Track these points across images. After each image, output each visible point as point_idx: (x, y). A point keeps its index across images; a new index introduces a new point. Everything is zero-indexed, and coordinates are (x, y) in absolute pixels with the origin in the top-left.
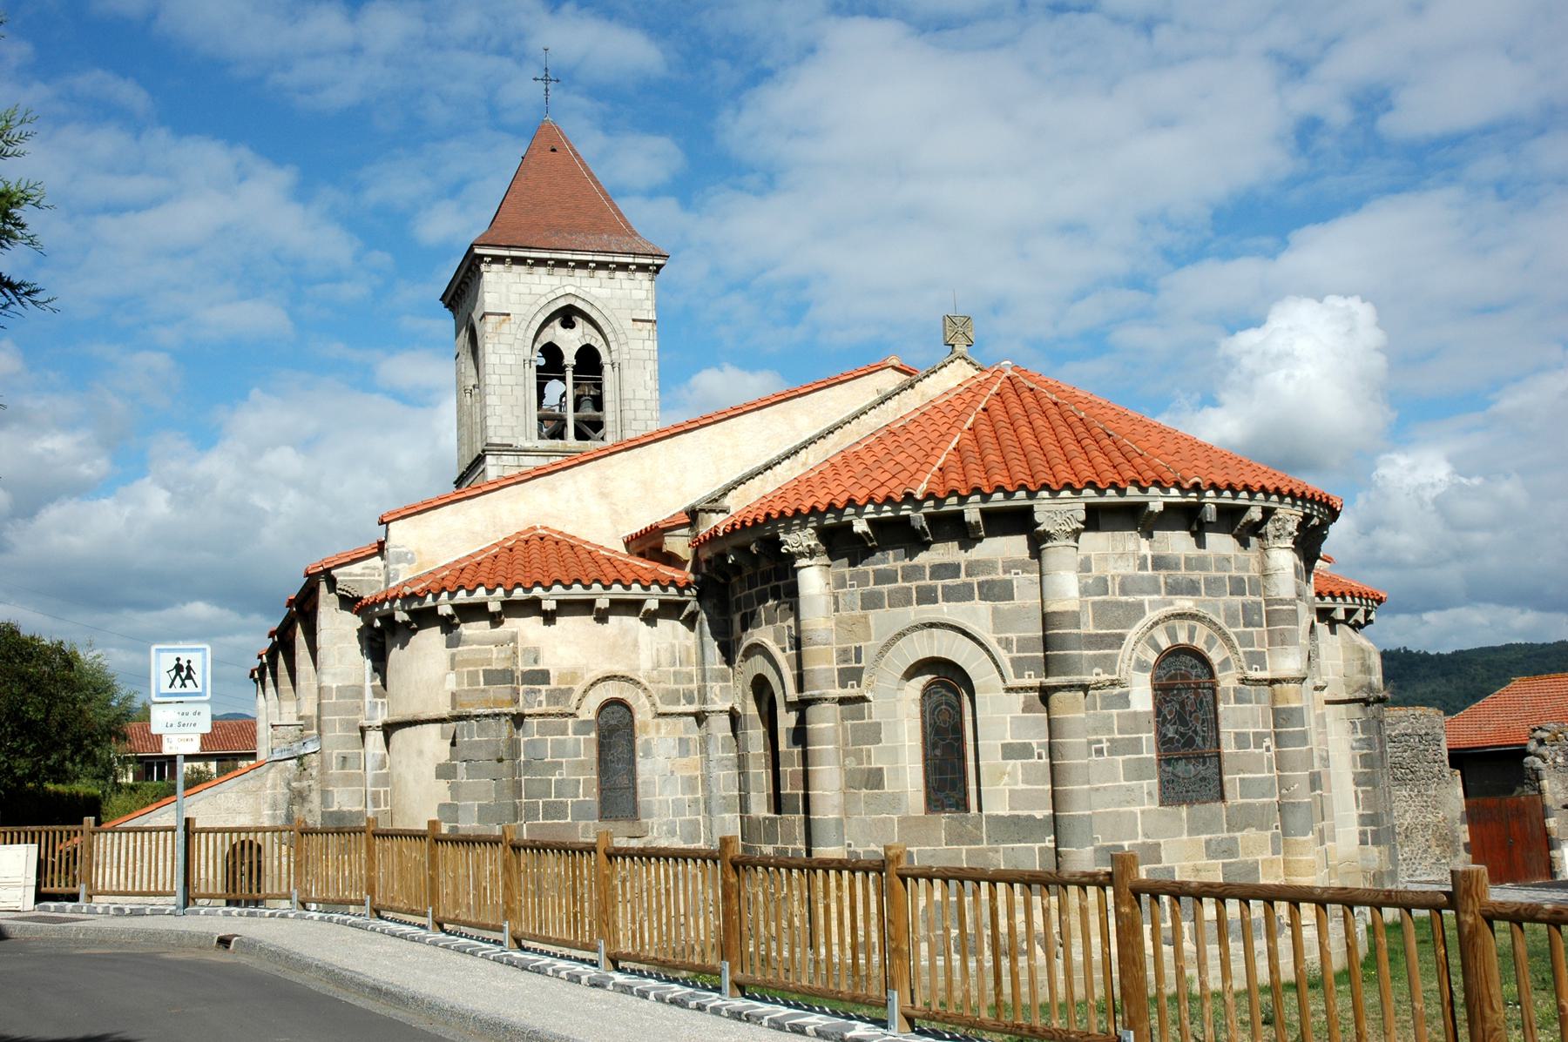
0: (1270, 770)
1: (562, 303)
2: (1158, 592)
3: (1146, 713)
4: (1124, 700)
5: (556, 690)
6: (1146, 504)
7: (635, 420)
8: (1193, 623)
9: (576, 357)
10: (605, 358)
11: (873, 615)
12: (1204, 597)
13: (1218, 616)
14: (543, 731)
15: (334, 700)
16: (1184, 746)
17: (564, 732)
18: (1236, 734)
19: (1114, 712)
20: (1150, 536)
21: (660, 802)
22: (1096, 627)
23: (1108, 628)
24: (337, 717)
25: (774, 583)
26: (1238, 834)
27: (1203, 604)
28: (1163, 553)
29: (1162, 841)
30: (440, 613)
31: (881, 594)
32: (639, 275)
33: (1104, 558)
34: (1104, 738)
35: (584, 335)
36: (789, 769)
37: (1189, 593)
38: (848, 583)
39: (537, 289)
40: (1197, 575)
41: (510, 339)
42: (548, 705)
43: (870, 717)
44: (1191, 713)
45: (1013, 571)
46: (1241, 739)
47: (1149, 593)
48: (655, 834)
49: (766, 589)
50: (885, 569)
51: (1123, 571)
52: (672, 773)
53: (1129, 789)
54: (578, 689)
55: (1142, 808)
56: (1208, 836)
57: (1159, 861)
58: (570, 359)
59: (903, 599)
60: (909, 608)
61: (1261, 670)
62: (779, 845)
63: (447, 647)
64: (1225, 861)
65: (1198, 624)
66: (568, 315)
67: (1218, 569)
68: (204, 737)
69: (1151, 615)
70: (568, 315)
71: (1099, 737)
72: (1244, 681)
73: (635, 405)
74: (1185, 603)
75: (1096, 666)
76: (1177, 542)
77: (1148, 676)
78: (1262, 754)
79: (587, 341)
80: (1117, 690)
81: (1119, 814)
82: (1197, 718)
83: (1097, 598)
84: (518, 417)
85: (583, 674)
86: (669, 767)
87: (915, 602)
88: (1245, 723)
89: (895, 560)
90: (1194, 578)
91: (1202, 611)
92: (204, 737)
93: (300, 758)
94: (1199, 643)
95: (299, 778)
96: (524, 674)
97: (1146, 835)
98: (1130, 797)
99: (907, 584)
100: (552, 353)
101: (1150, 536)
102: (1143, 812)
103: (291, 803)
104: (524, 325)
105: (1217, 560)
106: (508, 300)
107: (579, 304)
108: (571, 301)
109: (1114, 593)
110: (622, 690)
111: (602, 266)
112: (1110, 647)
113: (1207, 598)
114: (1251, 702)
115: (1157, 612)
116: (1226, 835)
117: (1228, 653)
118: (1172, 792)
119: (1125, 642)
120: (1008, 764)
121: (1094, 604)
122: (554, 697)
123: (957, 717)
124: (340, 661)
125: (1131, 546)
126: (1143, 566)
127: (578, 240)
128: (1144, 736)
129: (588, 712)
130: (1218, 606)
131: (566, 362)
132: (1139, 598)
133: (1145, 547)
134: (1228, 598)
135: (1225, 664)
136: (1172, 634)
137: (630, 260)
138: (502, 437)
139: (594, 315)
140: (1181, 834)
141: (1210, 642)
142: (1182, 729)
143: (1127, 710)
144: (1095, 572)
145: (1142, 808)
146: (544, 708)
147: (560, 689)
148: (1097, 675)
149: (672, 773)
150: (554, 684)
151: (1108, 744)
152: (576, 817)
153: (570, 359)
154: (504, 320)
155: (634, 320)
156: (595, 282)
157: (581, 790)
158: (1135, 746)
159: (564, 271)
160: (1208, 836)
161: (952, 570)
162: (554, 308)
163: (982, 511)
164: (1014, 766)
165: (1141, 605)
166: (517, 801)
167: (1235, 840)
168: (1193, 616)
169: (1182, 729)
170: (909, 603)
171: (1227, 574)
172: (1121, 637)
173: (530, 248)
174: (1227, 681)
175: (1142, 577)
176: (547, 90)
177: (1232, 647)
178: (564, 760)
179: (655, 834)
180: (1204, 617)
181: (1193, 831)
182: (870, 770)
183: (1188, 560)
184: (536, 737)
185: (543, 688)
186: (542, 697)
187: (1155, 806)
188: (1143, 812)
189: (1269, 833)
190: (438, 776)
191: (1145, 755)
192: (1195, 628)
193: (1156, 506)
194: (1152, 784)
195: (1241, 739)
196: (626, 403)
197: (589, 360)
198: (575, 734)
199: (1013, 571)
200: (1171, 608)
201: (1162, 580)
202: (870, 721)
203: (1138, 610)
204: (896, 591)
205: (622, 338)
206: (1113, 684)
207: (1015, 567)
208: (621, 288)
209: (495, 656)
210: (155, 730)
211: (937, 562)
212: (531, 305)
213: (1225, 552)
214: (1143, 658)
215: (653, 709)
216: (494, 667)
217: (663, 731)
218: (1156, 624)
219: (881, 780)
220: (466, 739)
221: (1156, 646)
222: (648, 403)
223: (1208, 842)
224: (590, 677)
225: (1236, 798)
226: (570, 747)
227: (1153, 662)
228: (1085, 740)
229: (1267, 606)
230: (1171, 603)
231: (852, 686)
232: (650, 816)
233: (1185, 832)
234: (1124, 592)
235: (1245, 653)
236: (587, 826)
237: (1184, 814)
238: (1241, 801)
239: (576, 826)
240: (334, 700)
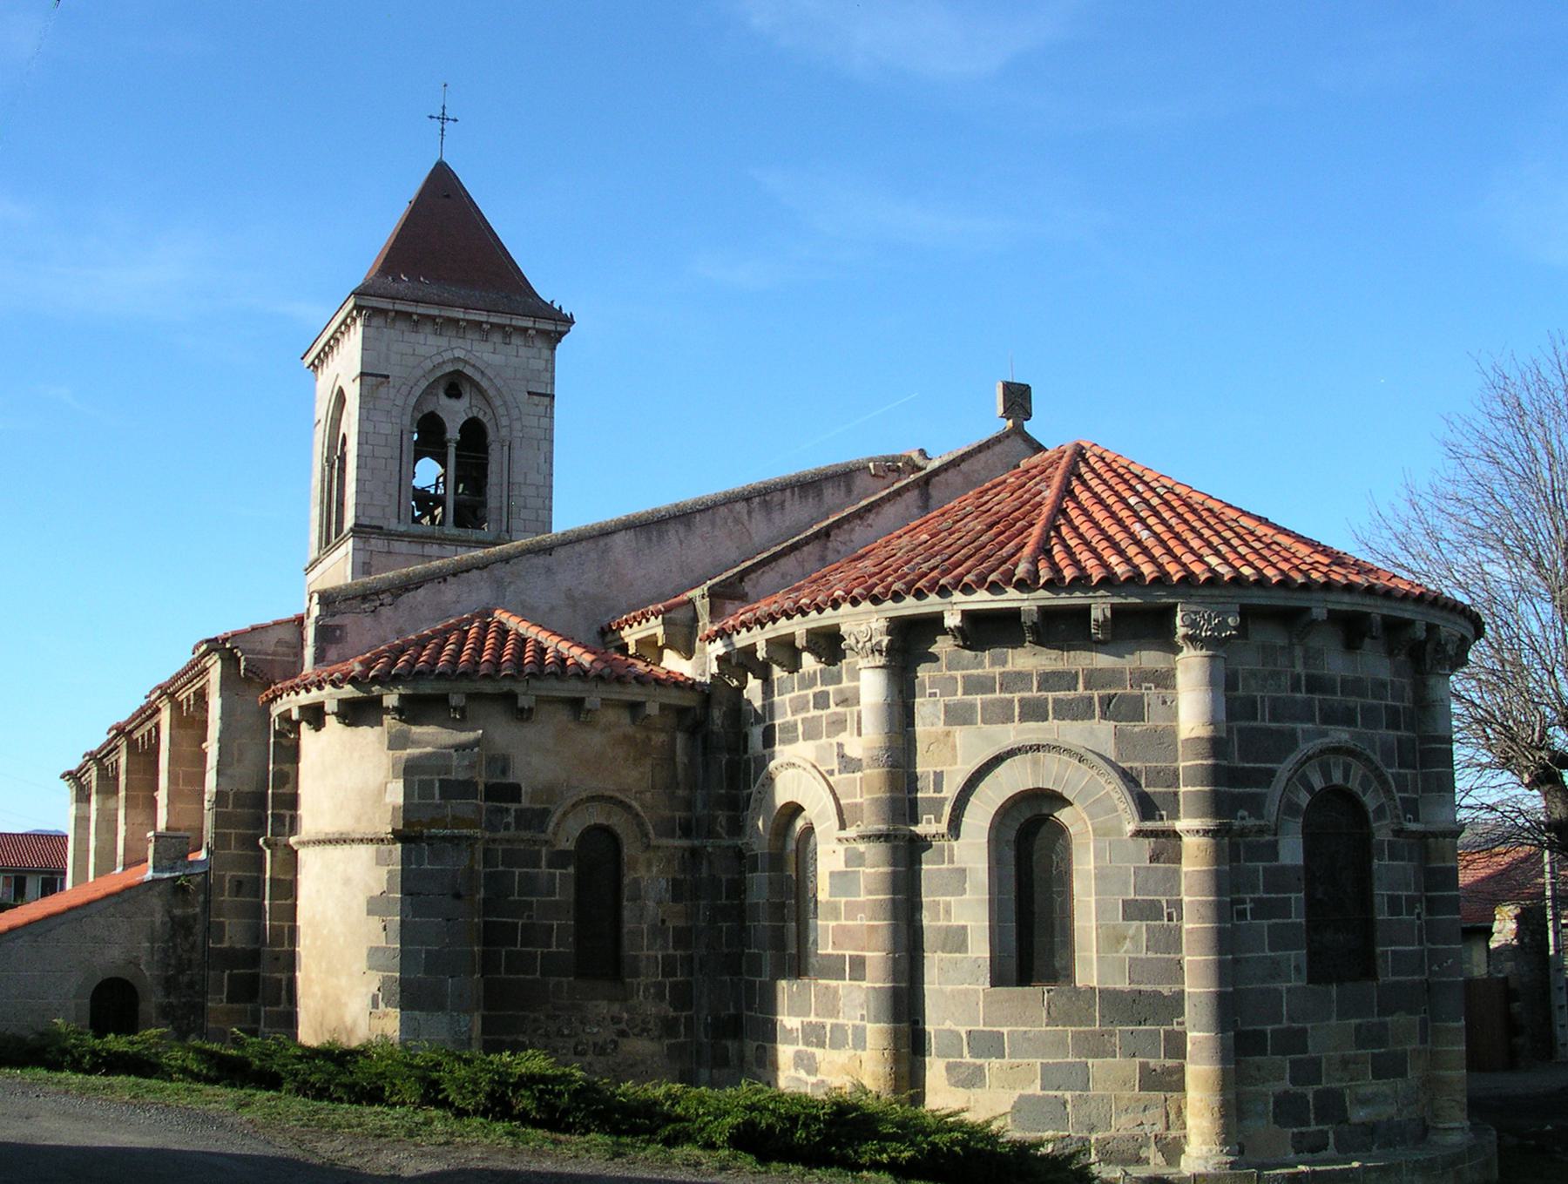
0: (1421, 943)
2: (1311, 719)
3: (1294, 867)
4: (1272, 851)
5: (528, 809)
7: (525, 507)
9: (460, 431)
10: (491, 436)
11: (959, 733)
15: (230, 808)
21: (648, 957)
23: (1255, 761)
24: (233, 831)
25: (818, 688)
26: (1388, 1019)
29: (1309, 1026)
30: (385, 704)
31: (972, 706)
34: (1248, 897)
35: (471, 407)
36: (832, 923)
38: (928, 691)
39: (421, 350)
40: (1354, 701)
42: (517, 828)
43: (951, 861)
45: (1144, 685)
48: (641, 998)
49: (807, 695)
50: (979, 676)
52: (663, 921)
53: (1275, 962)
55: (1289, 985)
56: (1358, 1021)
58: (453, 433)
59: (1002, 714)
60: (1010, 726)
61: (1414, 821)
62: (813, 1019)
63: (389, 748)
64: (1376, 1051)
66: (454, 385)
67: (1374, 697)
69: (1306, 747)
70: (454, 385)
71: (1241, 896)
74: (1341, 735)
75: (1241, 807)
79: (475, 412)
84: (391, 495)
85: (562, 793)
86: (660, 915)
87: (1017, 719)
89: (993, 664)
90: (1351, 705)
94: (1354, 785)
97: (1291, 1019)
99: (1008, 696)
102: (1289, 990)
104: (405, 390)
106: (387, 359)
107: (468, 371)
108: (460, 367)
109: (1263, 720)
110: (609, 815)
112: (1258, 784)
113: (1364, 730)
115: (1311, 744)
116: (1376, 1020)
118: (1321, 969)
119: (1275, 779)
120: (1131, 926)
124: (239, 761)
126: (1295, 687)
128: (1293, 895)
131: (448, 436)
134: (1383, 731)
138: (372, 518)
139: (484, 384)
143: (1274, 863)
145: (1289, 985)
147: (533, 809)
148: (1243, 818)
149: (663, 921)
150: (525, 802)
151: (1252, 905)
153: (453, 433)
154: (382, 383)
155: (529, 393)
156: (489, 346)
157: (554, 939)
158: (1281, 908)
160: (1358, 1021)
164: (1139, 929)
165: (1293, 733)
170: (1010, 719)
172: (1271, 774)
176: (443, 130)
177: (1388, 791)
178: (534, 899)
179: (641, 998)
180: (1362, 753)
182: (948, 929)
184: (501, 868)
185: (513, 806)
186: (511, 819)
187: (1302, 983)
190: (370, 912)
191: (1293, 920)
192: (1350, 765)
194: (1297, 956)
195: (1394, 905)
197: (474, 433)
198: (550, 866)
199: (1144, 685)
200: (1327, 740)
202: (951, 866)
203: (1287, 742)
204: (993, 703)
205: (514, 413)
207: (1146, 680)
208: (517, 356)
209: (455, 763)
211: (1049, 669)
212: (414, 367)
215: (644, 840)
216: (452, 777)
217: (655, 869)
218: (1309, 758)
219: (965, 941)
220: (414, 866)
221: (1309, 788)
222: (541, 490)
223: (1358, 1027)
225: (1387, 976)
228: (1228, 899)
229: (1420, 744)
230: (1325, 734)
231: (929, 821)
232: (636, 974)
233: (1335, 1015)
235: (1400, 798)
240: (230, 808)
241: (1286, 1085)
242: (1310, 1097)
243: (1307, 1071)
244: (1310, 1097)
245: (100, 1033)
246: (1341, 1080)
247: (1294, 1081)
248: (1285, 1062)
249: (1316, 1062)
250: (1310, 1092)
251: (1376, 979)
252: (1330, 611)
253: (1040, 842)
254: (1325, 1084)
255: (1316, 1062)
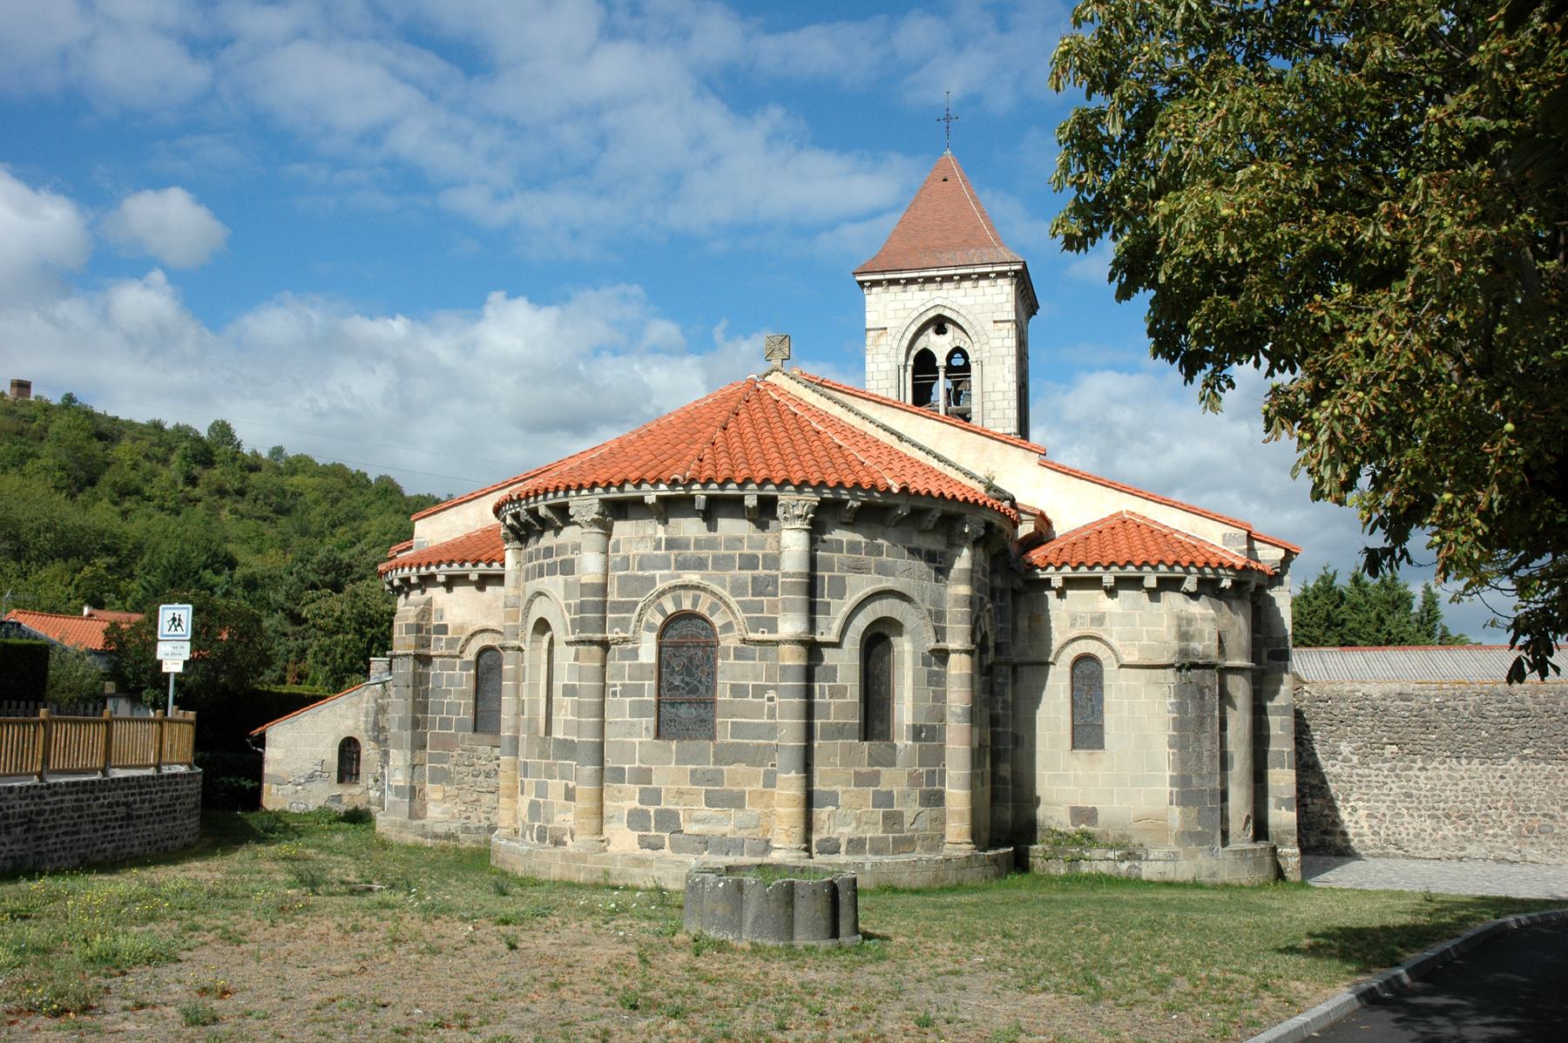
1: (932, 314)
2: (668, 568)
3: (650, 665)
4: (634, 654)
6: (642, 498)
8: (698, 592)
12: (710, 571)
13: (724, 587)
14: (443, 667)
16: (688, 693)
17: (454, 669)
18: (732, 685)
19: (627, 662)
20: (666, 522)
22: (619, 596)
26: (725, 768)
27: (710, 578)
28: (677, 536)
32: (1000, 281)
33: (629, 541)
34: (618, 683)
37: (695, 569)
39: (909, 305)
40: (704, 553)
41: (886, 349)
44: (697, 667)
46: (738, 691)
47: (661, 569)
51: (642, 551)
53: (632, 724)
54: (464, 638)
57: (650, 783)
65: (702, 594)
66: (940, 324)
67: (727, 548)
68: (185, 662)
69: (660, 586)
70: (940, 324)
72: (744, 641)
73: (994, 397)
74: (692, 577)
76: (690, 528)
77: (654, 635)
78: (762, 704)
80: (630, 646)
81: (624, 743)
82: (703, 672)
83: (621, 573)
88: (745, 677)
91: (705, 583)
92: (185, 662)
93: (383, 683)
95: (382, 697)
96: (435, 627)
97: (641, 761)
98: (631, 730)
100: (925, 361)
101: (666, 522)
102: (640, 743)
103: (377, 714)
105: (726, 540)
107: (947, 313)
108: (940, 311)
111: (964, 277)
114: (754, 659)
117: (731, 618)
121: (619, 577)
122: (451, 643)
123: (1078, 685)
125: (650, 531)
126: (658, 547)
127: (945, 258)
128: (647, 683)
129: (470, 655)
130: (718, 582)
132: (652, 572)
133: (661, 532)
134: (736, 572)
135: (728, 627)
136: (678, 602)
137: (1006, 268)
139: (960, 321)
140: (670, 763)
141: (713, 609)
142: (687, 679)
144: (622, 553)
146: (445, 652)
150: (450, 635)
152: (458, 729)
156: (960, 292)
158: (639, 690)
159: (933, 286)
161: (548, 552)
162: (924, 319)
163: (759, 498)
165: (653, 579)
166: (419, 716)
167: (721, 772)
168: (697, 588)
169: (687, 679)
171: (738, 552)
173: (900, 270)
174: (728, 641)
175: (657, 556)
181: (681, 760)
183: (697, 541)
185: (444, 637)
186: (443, 644)
188: (640, 743)
189: (762, 770)
193: (650, 499)
194: (650, 721)
196: (986, 395)
201: (673, 557)
206: (625, 640)
210: (159, 658)
213: (738, 534)
214: (652, 620)
221: (663, 612)
223: (693, 772)
224: (471, 630)
226: (457, 679)
227: (659, 624)
230: (679, 577)
234: (641, 568)
236: (463, 736)
237: (674, 747)
238: (730, 740)
239: (457, 737)
241: (636, 804)
242: (652, 813)
243: (651, 796)
244: (652, 813)
245: (1077, 826)
246: (676, 804)
247: (641, 802)
248: (636, 788)
249: (658, 792)
250: (652, 809)
251: (712, 737)
252: (658, 497)
253: (879, 649)
254: (663, 806)
255: (658, 792)
